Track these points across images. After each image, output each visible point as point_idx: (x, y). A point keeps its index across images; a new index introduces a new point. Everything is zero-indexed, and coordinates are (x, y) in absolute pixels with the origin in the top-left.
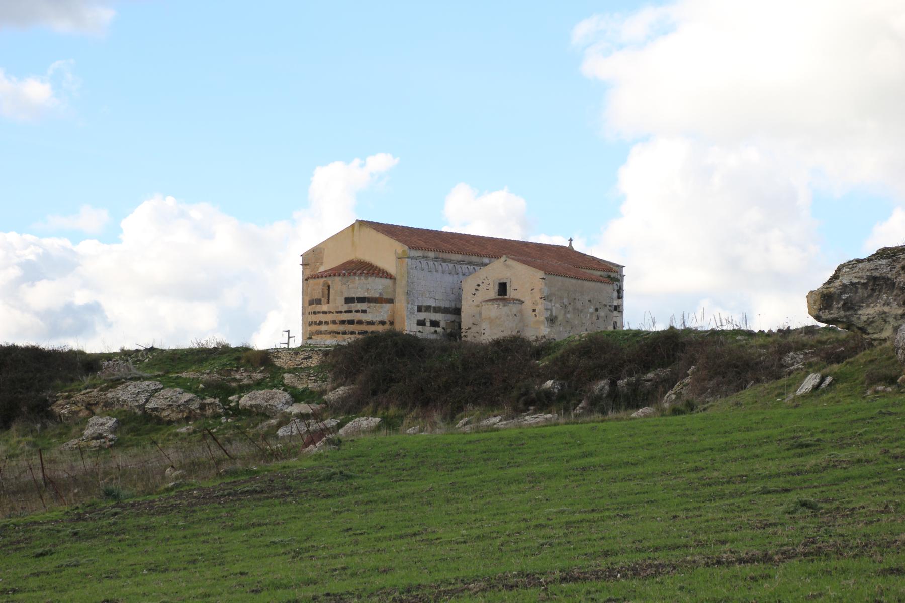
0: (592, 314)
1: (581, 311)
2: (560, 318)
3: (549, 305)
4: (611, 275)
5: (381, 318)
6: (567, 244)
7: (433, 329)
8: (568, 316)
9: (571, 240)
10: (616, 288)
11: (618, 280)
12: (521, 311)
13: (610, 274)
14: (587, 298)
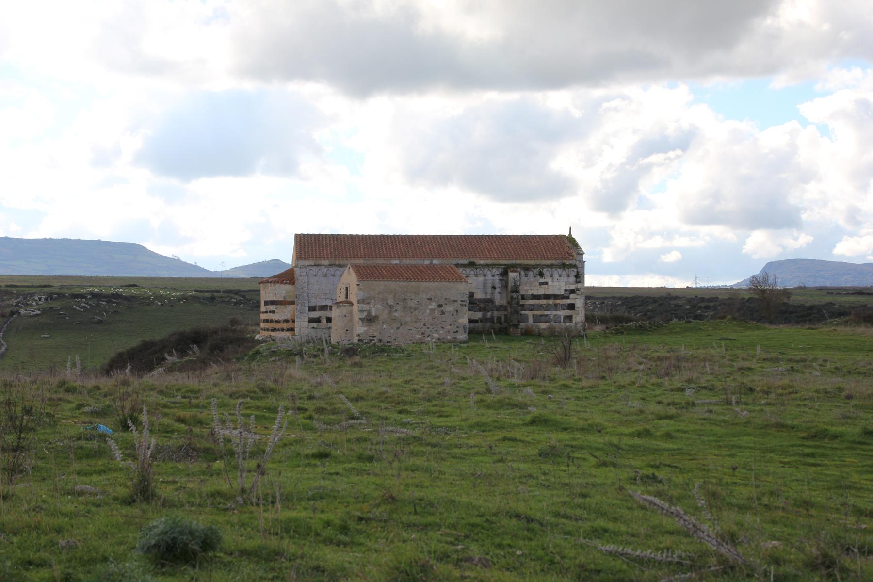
0: (432, 310)
1: (416, 309)
3: (366, 307)
5: (285, 318)
8: (396, 314)
11: (575, 266)
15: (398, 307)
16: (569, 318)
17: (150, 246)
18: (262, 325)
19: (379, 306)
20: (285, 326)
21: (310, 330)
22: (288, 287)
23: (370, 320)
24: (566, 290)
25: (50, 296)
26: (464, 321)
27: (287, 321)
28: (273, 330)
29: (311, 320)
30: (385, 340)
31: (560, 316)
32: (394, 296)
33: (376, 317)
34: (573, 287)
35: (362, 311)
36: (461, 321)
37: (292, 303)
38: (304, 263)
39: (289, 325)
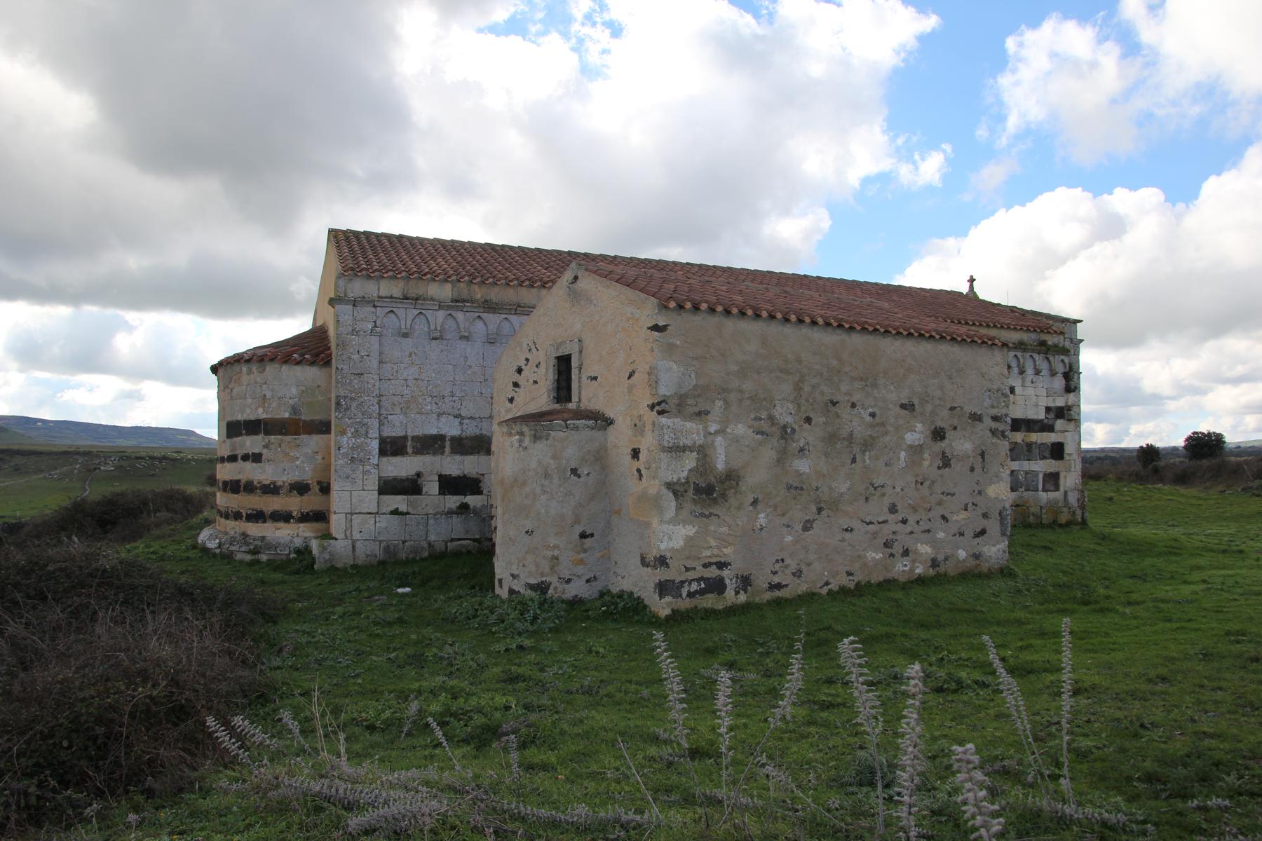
0: (916, 450)
1: (867, 445)
2: (758, 475)
3: (692, 431)
4: (1047, 341)
5: (294, 476)
6: (964, 289)
7: (453, 501)
8: (803, 466)
9: (972, 280)
10: (1060, 369)
11: (1065, 351)
12: (600, 458)
13: (1044, 337)
14: (894, 396)
15: (807, 436)
16: (1053, 479)
17: (198, 431)
18: (222, 499)
19: (740, 429)
20: (294, 504)
21: (384, 521)
22: (310, 374)
23: (707, 491)
24: (1048, 409)
25: (121, 458)
26: (1000, 492)
27: (301, 488)
28: (257, 516)
29: (389, 487)
30: (761, 580)
31: (1036, 474)
32: (798, 388)
33: (731, 477)
34: (1060, 402)
35: (677, 450)
36: (992, 491)
37: (323, 427)
38: (370, 288)
39: (311, 502)
